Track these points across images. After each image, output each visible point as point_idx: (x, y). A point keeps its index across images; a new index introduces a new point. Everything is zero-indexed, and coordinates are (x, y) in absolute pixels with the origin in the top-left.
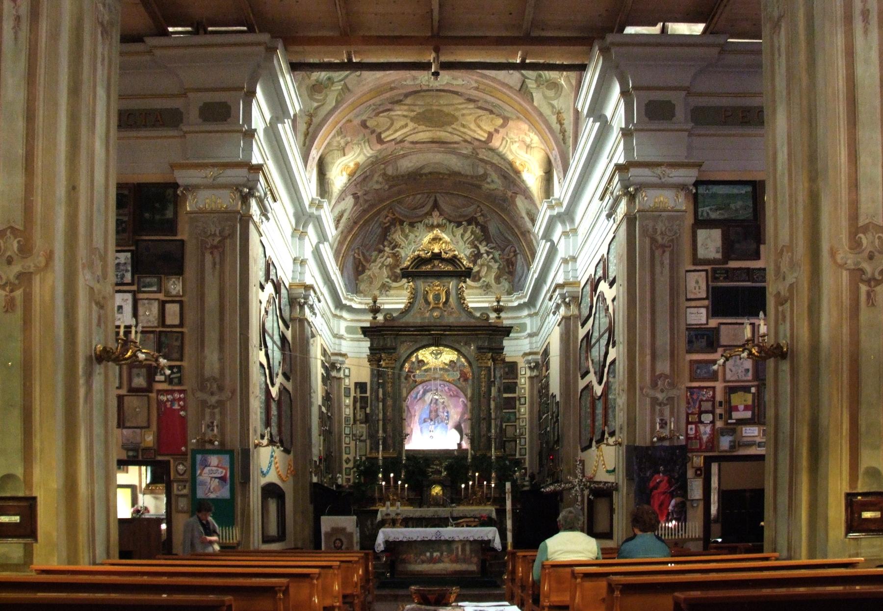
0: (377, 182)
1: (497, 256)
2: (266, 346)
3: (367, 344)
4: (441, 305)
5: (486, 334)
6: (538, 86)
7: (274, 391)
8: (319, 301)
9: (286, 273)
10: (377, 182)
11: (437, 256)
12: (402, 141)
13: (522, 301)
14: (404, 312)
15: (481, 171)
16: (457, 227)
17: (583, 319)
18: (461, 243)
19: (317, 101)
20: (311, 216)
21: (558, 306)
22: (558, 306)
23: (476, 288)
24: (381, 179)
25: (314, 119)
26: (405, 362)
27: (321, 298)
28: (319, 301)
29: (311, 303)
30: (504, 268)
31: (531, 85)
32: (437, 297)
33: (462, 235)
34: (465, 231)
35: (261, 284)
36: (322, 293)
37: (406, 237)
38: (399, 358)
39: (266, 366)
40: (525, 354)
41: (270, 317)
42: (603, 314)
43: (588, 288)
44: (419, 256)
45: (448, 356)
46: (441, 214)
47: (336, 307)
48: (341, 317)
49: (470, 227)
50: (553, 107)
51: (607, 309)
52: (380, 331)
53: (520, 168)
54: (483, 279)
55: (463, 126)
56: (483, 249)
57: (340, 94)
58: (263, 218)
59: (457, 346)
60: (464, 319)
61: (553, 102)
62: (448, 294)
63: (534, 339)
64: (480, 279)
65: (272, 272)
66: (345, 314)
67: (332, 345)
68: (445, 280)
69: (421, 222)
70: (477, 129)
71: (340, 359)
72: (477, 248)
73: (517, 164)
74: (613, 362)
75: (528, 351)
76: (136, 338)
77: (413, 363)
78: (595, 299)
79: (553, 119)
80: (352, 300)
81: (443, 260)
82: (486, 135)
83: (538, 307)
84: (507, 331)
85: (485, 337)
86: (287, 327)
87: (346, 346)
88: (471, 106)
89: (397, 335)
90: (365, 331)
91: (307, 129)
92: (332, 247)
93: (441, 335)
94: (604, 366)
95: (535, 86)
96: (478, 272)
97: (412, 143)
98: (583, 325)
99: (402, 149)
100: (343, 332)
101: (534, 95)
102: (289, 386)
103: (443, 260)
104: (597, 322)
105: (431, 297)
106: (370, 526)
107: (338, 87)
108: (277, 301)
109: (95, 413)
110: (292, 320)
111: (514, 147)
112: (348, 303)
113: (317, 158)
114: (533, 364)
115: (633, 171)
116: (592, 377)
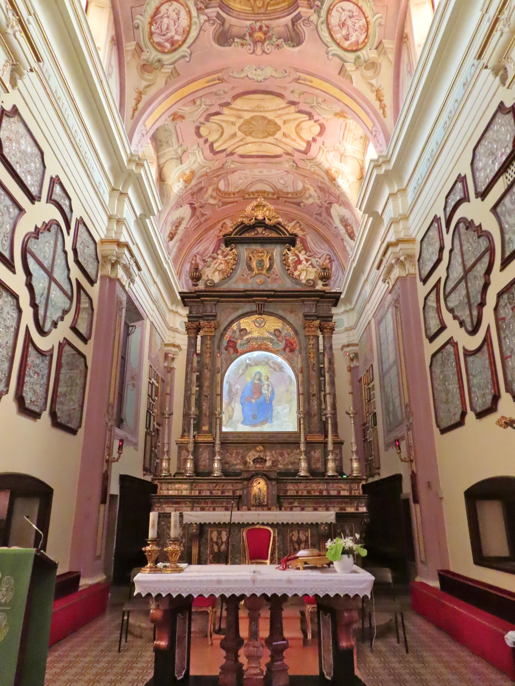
0: (212, 196)
1: (315, 264)
3: (184, 312)
4: (264, 272)
5: (314, 301)
6: (357, 68)
10: (212, 196)
11: (261, 223)
15: (300, 186)
20: (130, 174)
24: (214, 194)
25: (143, 96)
28: (139, 269)
31: (350, 67)
32: (261, 262)
38: (219, 326)
40: (344, 347)
44: (242, 223)
45: (272, 324)
47: (172, 303)
50: (372, 85)
53: (335, 175)
55: (285, 135)
59: (281, 313)
61: (370, 81)
63: (351, 333)
68: (269, 247)
70: (297, 139)
71: (174, 349)
73: (333, 172)
77: (234, 332)
79: (372, 97)
81: (266, 227)
82: (305, 145)
83: (354, 303)
88: (293, 109)
89: (218, 301)
91: (136, 105)
93: (266, 301)
95: (354, 68)
97: (242, 156)
101: (353, 77)
103: (266, 227)
105: (254, 264)
107: (167, 70)
109: (419, 515)
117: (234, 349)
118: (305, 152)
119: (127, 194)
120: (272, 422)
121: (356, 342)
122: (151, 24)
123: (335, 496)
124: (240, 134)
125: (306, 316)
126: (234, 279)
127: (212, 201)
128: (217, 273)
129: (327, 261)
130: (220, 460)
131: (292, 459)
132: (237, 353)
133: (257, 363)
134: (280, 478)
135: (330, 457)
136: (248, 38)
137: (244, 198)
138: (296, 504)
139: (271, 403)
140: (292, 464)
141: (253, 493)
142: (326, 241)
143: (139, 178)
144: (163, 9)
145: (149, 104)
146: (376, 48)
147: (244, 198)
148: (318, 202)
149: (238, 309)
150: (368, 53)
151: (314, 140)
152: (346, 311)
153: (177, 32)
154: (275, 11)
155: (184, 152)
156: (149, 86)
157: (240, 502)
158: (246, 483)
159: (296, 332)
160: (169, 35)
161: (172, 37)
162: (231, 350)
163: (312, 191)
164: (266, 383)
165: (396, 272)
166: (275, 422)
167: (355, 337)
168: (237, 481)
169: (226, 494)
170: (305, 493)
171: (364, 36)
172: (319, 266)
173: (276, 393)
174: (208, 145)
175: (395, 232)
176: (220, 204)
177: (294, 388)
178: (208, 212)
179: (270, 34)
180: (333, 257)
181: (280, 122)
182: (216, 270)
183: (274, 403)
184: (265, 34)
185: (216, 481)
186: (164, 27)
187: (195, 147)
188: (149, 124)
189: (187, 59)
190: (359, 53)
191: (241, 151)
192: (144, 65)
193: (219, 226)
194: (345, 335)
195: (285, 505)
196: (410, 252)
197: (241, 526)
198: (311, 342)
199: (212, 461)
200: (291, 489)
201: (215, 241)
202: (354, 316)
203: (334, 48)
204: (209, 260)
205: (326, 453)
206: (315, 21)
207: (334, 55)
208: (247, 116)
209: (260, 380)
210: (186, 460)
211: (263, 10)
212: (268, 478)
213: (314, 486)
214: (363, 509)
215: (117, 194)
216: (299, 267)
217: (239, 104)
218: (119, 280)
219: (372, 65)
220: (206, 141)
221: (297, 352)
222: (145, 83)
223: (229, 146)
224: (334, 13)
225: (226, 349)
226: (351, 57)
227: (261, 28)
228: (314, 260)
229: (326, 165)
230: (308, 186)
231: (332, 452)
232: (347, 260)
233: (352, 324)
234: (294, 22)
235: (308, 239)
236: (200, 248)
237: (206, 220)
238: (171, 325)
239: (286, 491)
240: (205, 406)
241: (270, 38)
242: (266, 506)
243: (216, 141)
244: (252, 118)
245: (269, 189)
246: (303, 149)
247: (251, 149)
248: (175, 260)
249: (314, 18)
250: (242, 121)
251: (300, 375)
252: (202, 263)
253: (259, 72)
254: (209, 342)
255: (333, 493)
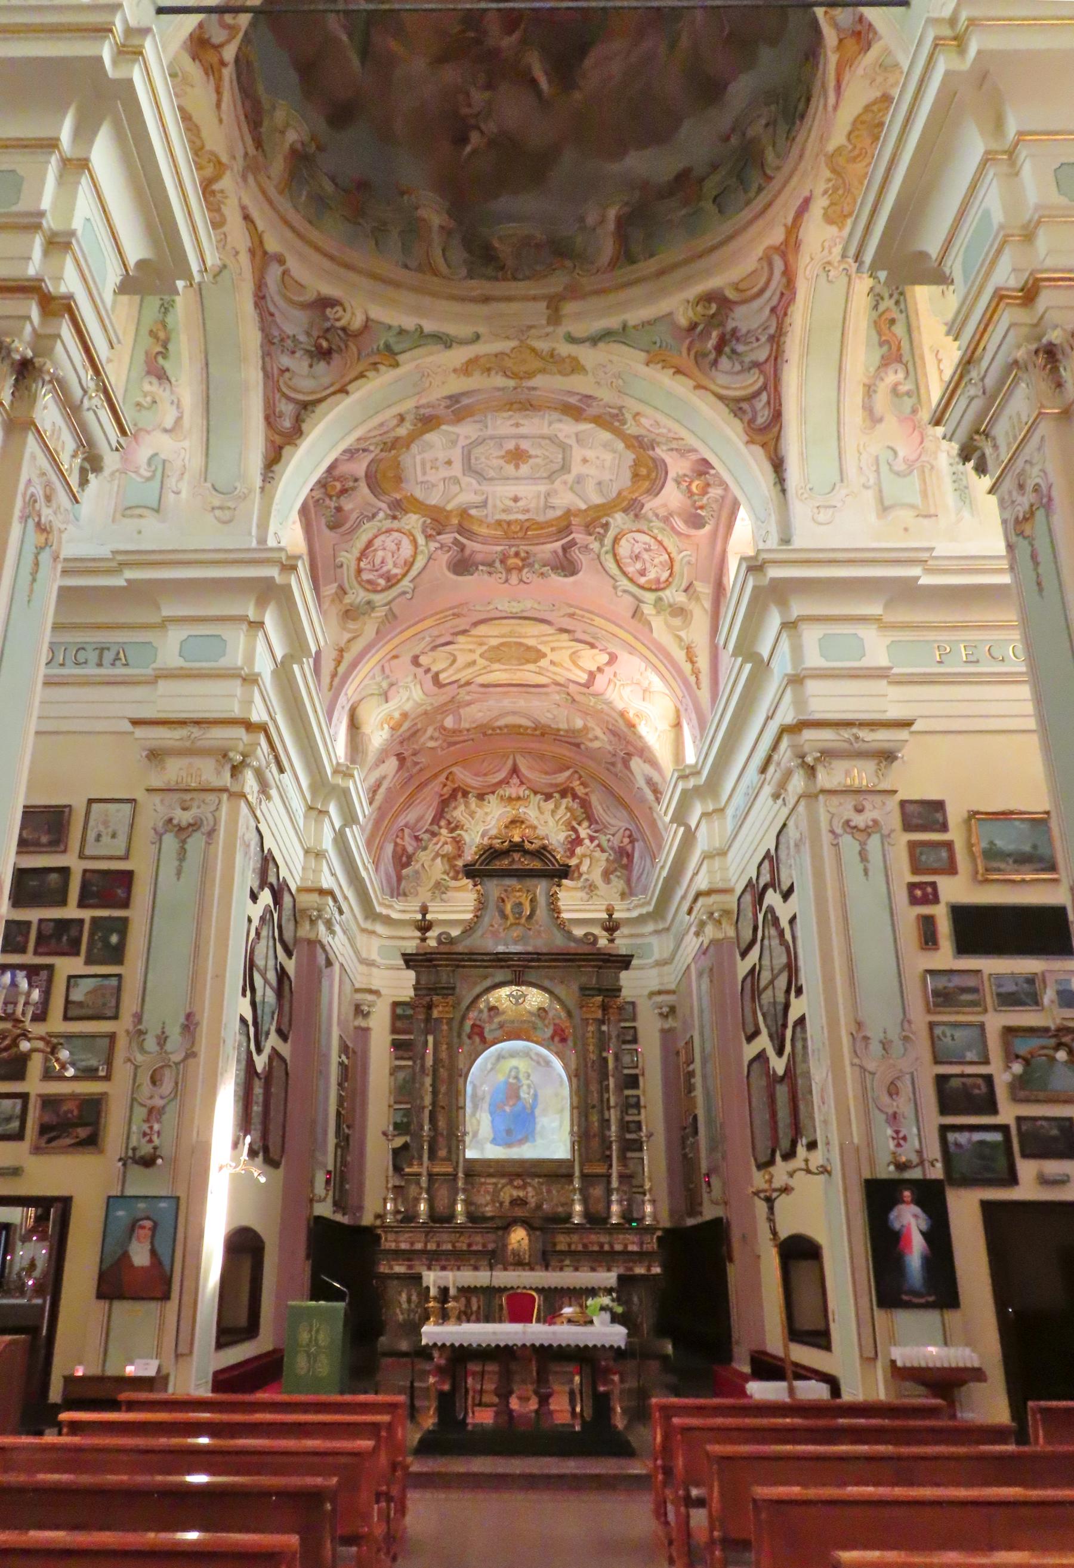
0: (432, 738)
1: (605, 844)
2: (253, 990)
4: (523, 921)
7: (260, 1062)
8: (341, 912)
9: (293, 869)
10: (432, 738)
12: (468, 683)
13: (644, 911)
14: (469, 929)
15: (579, 723)
16: (546, 801)
17: (743, 946)
18: (551, 822)
19: (349, 631)
20: (335, 788)
21: (702, 924)
22: (702, 924)
23: (575, 889)
24: (436, 734)
26: (468, 1008)
27: (345, 908)
28: (341, 912)
29: (327, 916)
30: (614, 861)
31: (648, 610)
33: (553, 812)
34: (557, 807)
35: (252, 891)
36: (346, 898)
37: (472, 814)
38: (459, 1004)
39: (250, 1022)
40: (652, 994)
41: (263, 942)
42: (775, 942)
43: (748, 898)
44: (491, 847)
45: (535, 998)
46: (522, 783)
47: (366, 918)
48: (373, 932)
49: (565, 801)
50: (680, 639)
51: (781, 934)
52: (430, 960)
53: (635, 721)
54: (584, 877)
55: (552, 662)
56: (584, 832)
57: (382, 622)
58: (263, 797)
59: (546, 983)
60: (559, 942)
62: (533, 901)
63: (666, 969)
64: (580, 875)
65: (272, 870)
66: (380, 929)
67: (360, 976)
68: (530, 882)
69: (493, 793)
71: (370, 997)
72: (574, 829)
73: (631, 715)
74: (801, 1021)
75: (656, 988)
76: (24, 1014)
77: (481, 1011)
78: (761, 917)
79: (680, 656)
80: (390, 907)
81: (526, 852)
84: (625, 962)
85: (592, 971)
86: (289, 953)
87: (379, 979)
88: (565, 636)
89: (458, 966)
90: (410, 960)
92: (363, 830)
94: (785, 1026)
95: (654, 612)
96: (578, 866)
97: (483, 686)
98: (744, 954)
99: (468, 693)
100: (374, 956)
102: (285, 1049)
103: (526, 852)
104: (766, 953)
105: (508, 907)
106: (405, 1306)
107: (380, 613)
108: (276, 916)
110: (296, 940)
111: (627, 692)
112: (384, 911)
113: (347, 708)
114: (665, 1010)
115: (808, 734)
116: (763, 1042)
117: (481, 1039)
118: (587, 685)
119: (327, 812)
120: (534, 1140)
121: (673, 987)
122: (359, 560)
123: (619, 1253)
124: (482, 662)
125: (583, 989)
126: (479, 933)
127: (431, 744)
128: (439, 860)
129: (626, 840)
130: (464, 1201)
131: (563, 1200)
132: (486, 1044)
133: (513, 1054)
134: (547, 1225)
135: (614, 1198)
136: (497, 564)
137: (485, 734)
138: (567, 1262)
139: (532, 1114)
140: (563, 1205)
141: (510, 1247)
142: (626, 807)
143: (346, 792)
144: (378, 542)
145: (354, 665)
146: (685, 591)
147: (485, 734)
148: (610, 748)
149: (486, 977)
150: (674, 595)
151: (600, 670)
152: (657, 932)
153: (395, 565)
154: (538, 536)
155: (392, 685)
156: (354, 638)
157: (495, 1258)
158: (500, 1233)
159: (569, 1014)
160: (385, 569)
161: (389, 571)
162: (477, 1039)
163: (599, 732)
164: (525, 1082)
165: (710, 932)
166: (539, 1141)
167: (670, 978)
168: (489, 1230)
169: (474, 1248)
170: (580, 1248)
171: (667, 574)
172: (612, 848)
173: (540, 1099)
174: (429, 675)
175: (709, 872)
176: (445, 745)
177: (566, 1091)
178: (422, 759)
179: (531, 560)
180: (636, 835)
181: (544, 649)
182: (437, 855)
183: (537, 1112)
184: (523, 560)
185: (460, 1230)
186: (378, 561)
187: (410, 678)
188: (350, 692)
189: (409, 596)
190: (660, 593)
191: (480, 680)
192: (347, 611)
193: (442, 778)
194: (654, 972)
195: (553, 1263)
196: (727, 907)
197: (501, 1290)
198: (591, 1028)
199: (454, 1203)
200: (562, 1242)
201: (435, 804)
202: (669, 942)
203: (624, 583)
204: (426, 837)
205: (609, 1192)
206: (596, 550)
207: (625, 591)
208: (494, 642)
209: (516, 1078)
210: (417, 1200)
211: (520, 535)
212: (526, 1223)
213: (593, 1237)
214: (657, 1270)
215: (314, 813)
216: (579, 850)
217: (482, 630)
218: (320, 942)
219: (679, 611)
220: (428, 671)
221: (570, 1043)
222: (347, 636)
223: (465, 675)
224: (623, 542)
225: (469, 1037)
226: (650, 597)
227: (517, 554)
228: (603, 839)
229: (620, 705)
230: (591, 724)
231: (618, 1190)
232: (660, 847)
233: (666, 955)
234: (565, 549)
235: (595, 800)
236: (411, 816)
237: (421, 770)
238: (364, 955)
239: (555, 1244)
240: (442, 1124)
241: (531, 565)
242: (529, 1264)
243: (443, 670)
244: (502, 644)
245: (524, 722)
246: (583, 681)
247: (499, 675)
248: (369, 843)
249: (595, 546)
250: (485, 648)
251: (574, 1080)
252: (414, 844)
253: (513, 604)
254: (445, 1027)
255: (618, 1247)
